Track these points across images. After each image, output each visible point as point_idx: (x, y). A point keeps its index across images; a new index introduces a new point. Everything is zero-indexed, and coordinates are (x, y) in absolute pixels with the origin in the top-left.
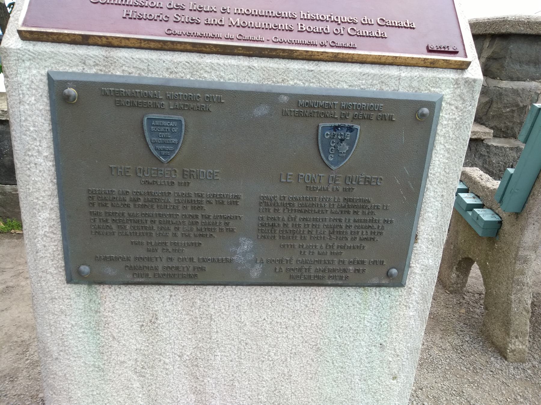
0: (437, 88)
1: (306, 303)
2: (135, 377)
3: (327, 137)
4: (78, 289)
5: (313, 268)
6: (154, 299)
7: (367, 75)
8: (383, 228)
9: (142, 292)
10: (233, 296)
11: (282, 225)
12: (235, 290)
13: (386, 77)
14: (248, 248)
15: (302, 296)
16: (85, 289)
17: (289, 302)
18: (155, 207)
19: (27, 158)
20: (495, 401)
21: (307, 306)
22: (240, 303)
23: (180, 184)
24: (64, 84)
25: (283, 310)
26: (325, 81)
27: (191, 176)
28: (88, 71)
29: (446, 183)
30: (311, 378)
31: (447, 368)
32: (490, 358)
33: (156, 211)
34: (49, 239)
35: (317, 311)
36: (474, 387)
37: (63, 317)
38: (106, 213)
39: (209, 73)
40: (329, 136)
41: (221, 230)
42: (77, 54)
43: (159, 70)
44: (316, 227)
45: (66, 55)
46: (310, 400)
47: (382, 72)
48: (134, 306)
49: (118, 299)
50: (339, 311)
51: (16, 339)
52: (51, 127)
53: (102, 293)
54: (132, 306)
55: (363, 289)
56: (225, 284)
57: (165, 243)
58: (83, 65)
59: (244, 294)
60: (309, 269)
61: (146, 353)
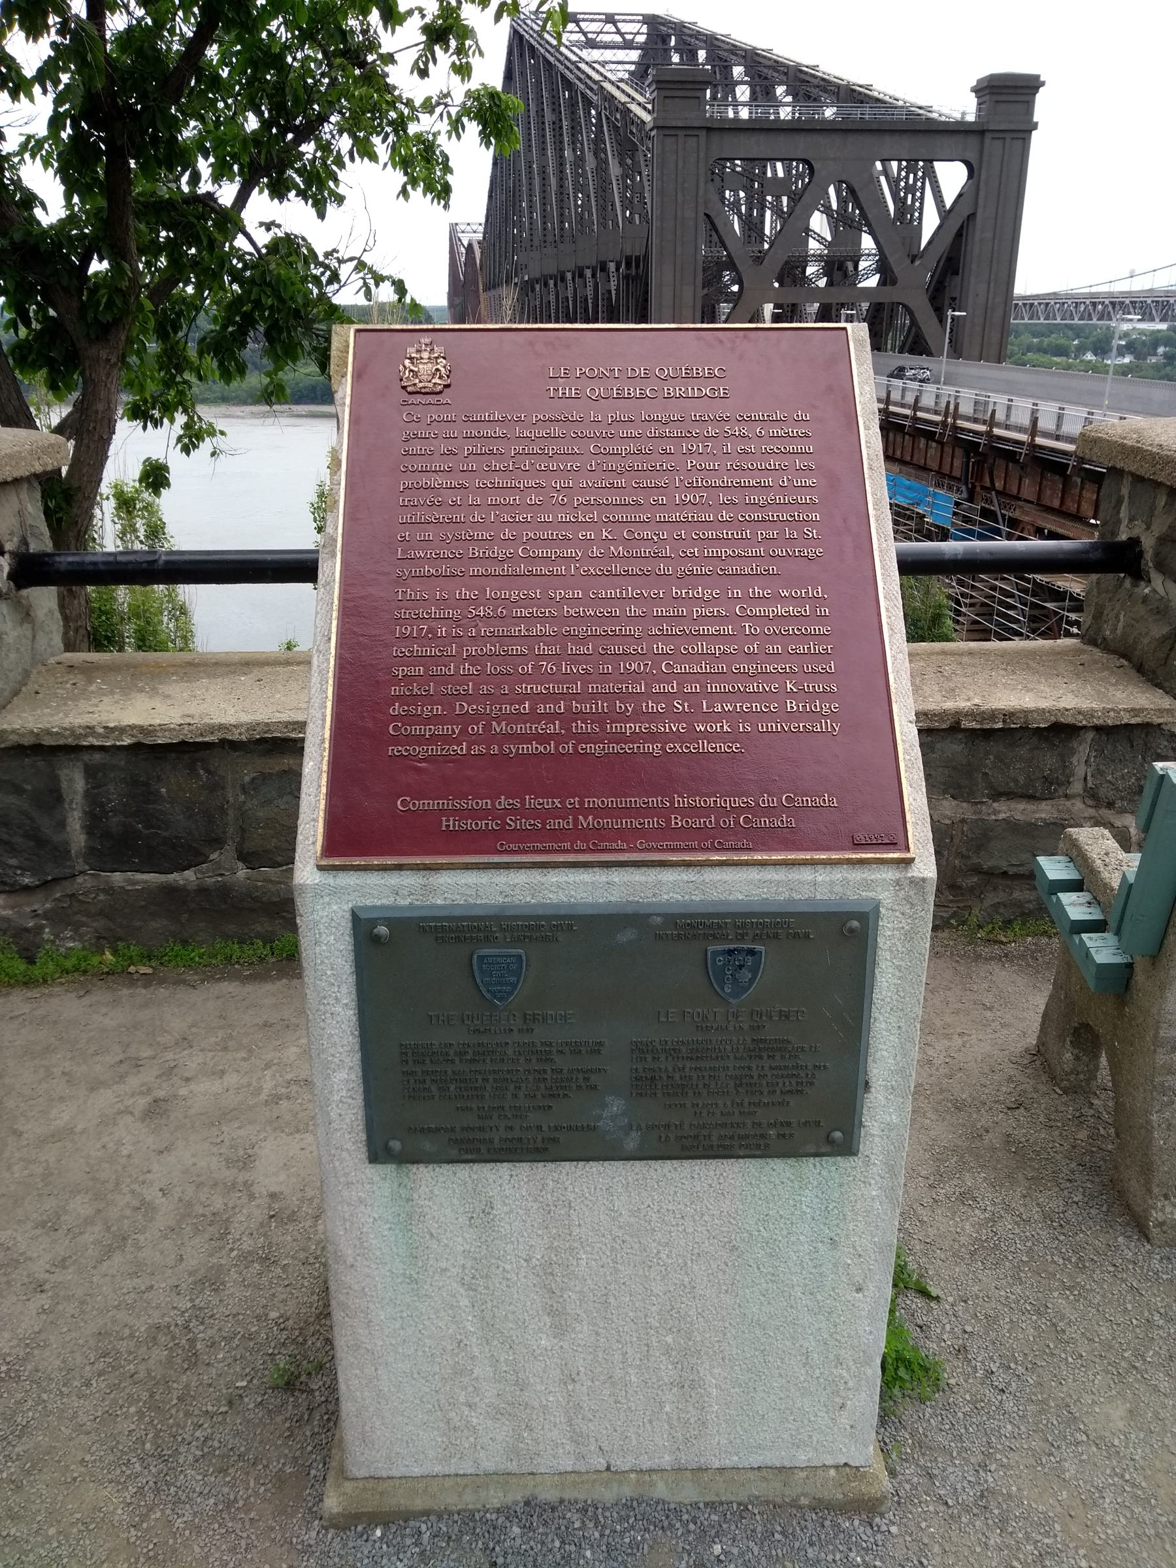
2: (462, 1291)
18: (488, 1061)
19: (322, 1007)
20: (1107, 1324)
24: (374, 922)
25: (676, 1193)
29: (902, 1010)
30: (727, 1291)
31: (1025, 1259)
32: (1116, 1238)
34: (346, 1106)
36: (1072, 1297)
37: (362, 1208)
38: (423, 1072)
41: (579, 1087)
46: (727, 1325)
47: (790, 877)
51: (201, 1211)
52: (353, 969)
56: (588, 1160)
57: (503, 1108)
61: (478, 1256)
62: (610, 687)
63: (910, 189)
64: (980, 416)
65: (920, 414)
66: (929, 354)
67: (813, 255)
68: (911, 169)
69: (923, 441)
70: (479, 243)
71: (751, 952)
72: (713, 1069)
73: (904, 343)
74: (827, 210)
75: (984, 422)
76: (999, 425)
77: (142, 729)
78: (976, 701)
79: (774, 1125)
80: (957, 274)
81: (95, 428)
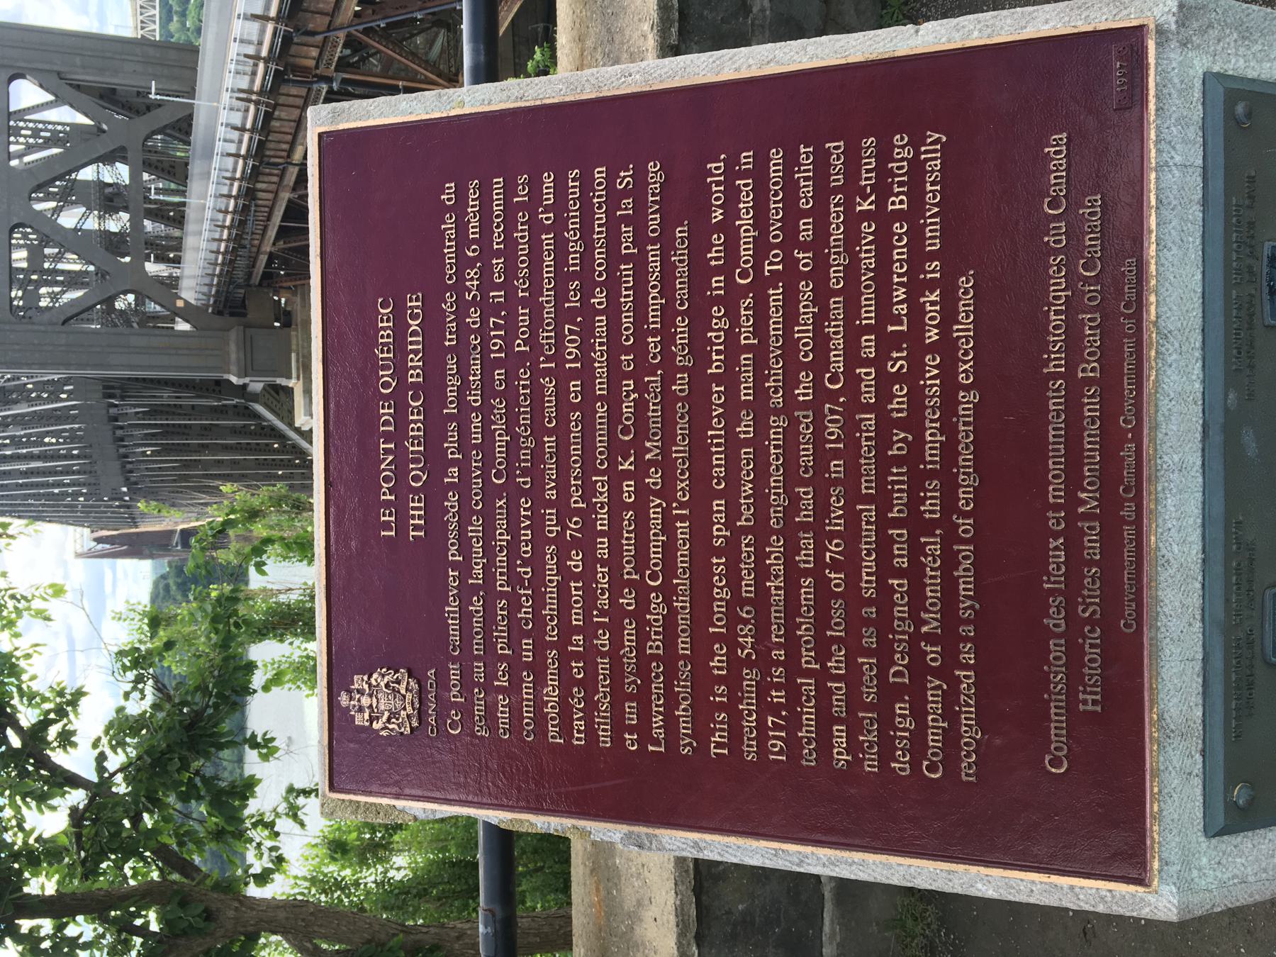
24: (1231, 806)
62: (868, 464)
63: (36, 133)
64: (249, 69)
65: (248, 126)
66: (190, 117)
67: (100, 224)
68: (16, 132)
69: (275, 124)
70: (92, 532)
73: (181, 140)
74: (57, 211)
75: (256, 65)
76: (259, 51)
77: (681, 935)
78: (646, 27)
80: (114, 90)
81: (303, 920)
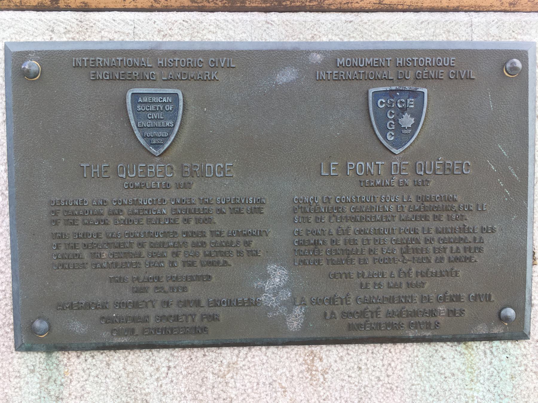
0: (525, 35)
1: (378, 374)
3: (381, 107)
4: (31, 361)
5: (384, 309)
6: (144, 374)
7: (426, 23)
8: (481, 241)
9: (126, 363)
10: (263, 364)
11: (329, 243)
12: (265, 355)
13: (453, 24)
14: (280, 281)
15: (371, 361)
16: (42, 360)
17: (350, 373)
21: (379, 380)
22: (274, 378)
23: (178, 186)
24: (23, 56)
25: (343, 387)
26: (370, 34)
27: (192, 173)
28: (55, 39)
33: (146, 228)
35: (397, 387)
39: (214, 33)
40: (384, 105)
41: (240, 253)
42: (43, 19)
43: (148, 33)
44: (379, 243)
45: (30, 22)
48: (113, 386)
49: (89, 376)
50: (431, 387)
53: (66, 365)
54: (110, 387)
55: (464, 346)
58: (51, 33)
59: (280, 361)
60: (376, 312)
71: (414, 94)
72: (378, 232)
79: (441, 300)
